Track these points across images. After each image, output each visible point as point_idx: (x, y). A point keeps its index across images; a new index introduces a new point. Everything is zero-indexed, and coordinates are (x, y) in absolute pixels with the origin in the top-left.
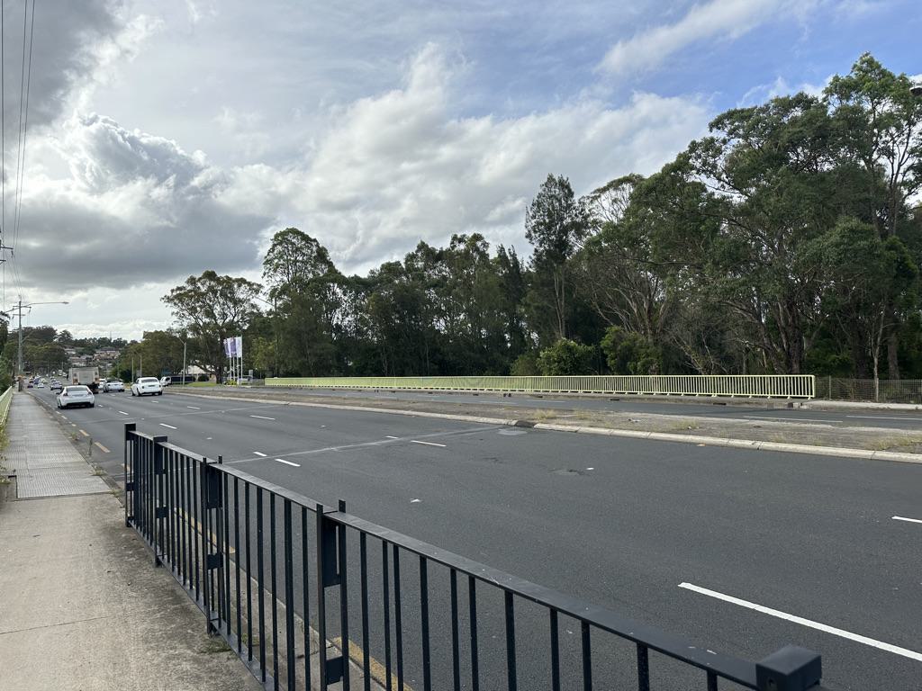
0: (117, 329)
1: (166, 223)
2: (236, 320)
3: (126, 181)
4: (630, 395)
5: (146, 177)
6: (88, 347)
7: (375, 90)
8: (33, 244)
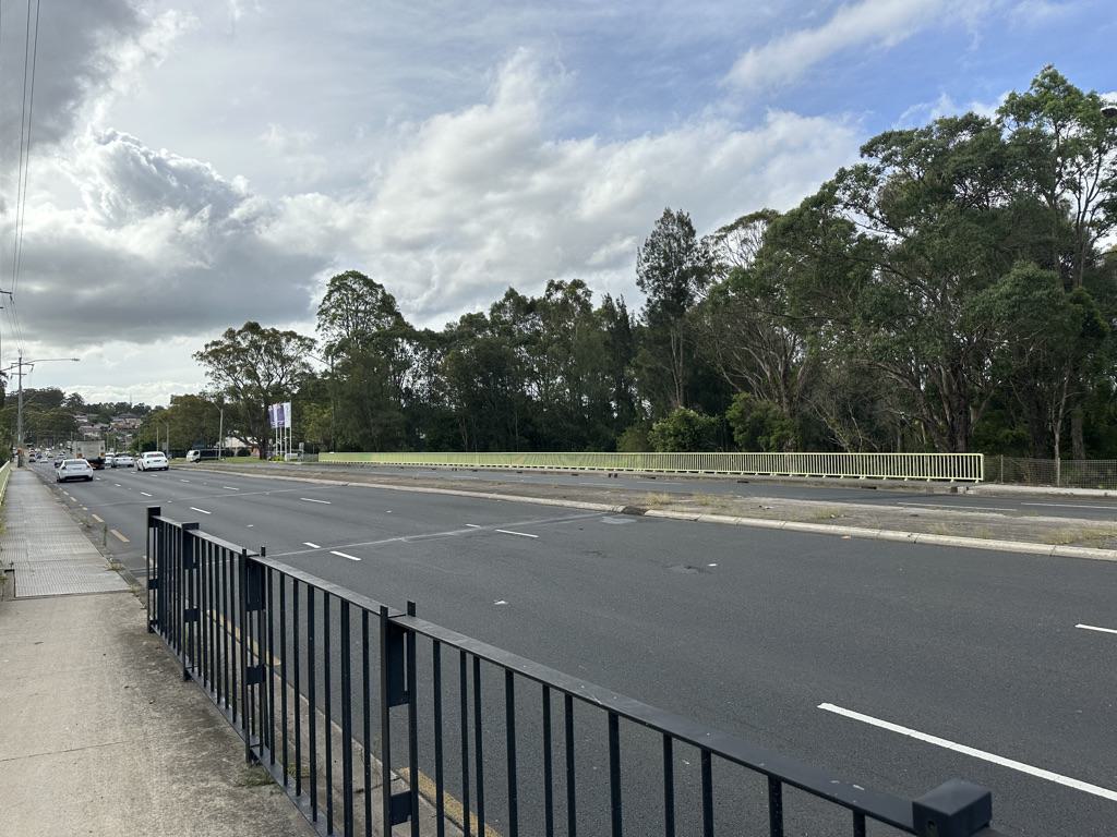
1: (199, 263)
2: (283, 382)
3: (151, 213)
5: (175, 207)
6: (101, 413)
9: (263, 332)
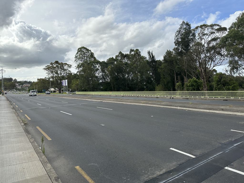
0: (29, 79)
1: (39, 50)
4: (163, 97)
6: (21, 83)
7: (95, 16)
8: (5, 56)
9: (59, 63)
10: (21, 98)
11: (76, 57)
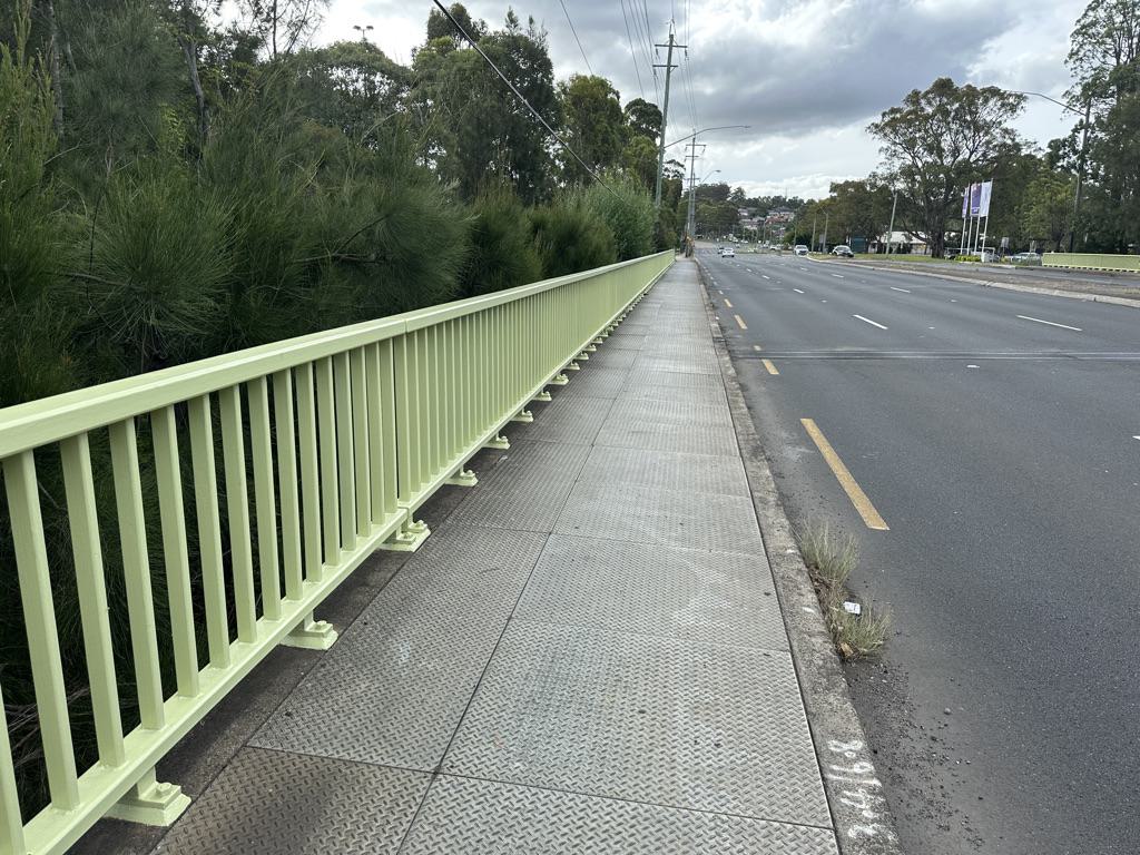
1: (845, 47)
2: (973, 158)
6: (761, 207)
10: (760, 274)
11: (1083, 31)
